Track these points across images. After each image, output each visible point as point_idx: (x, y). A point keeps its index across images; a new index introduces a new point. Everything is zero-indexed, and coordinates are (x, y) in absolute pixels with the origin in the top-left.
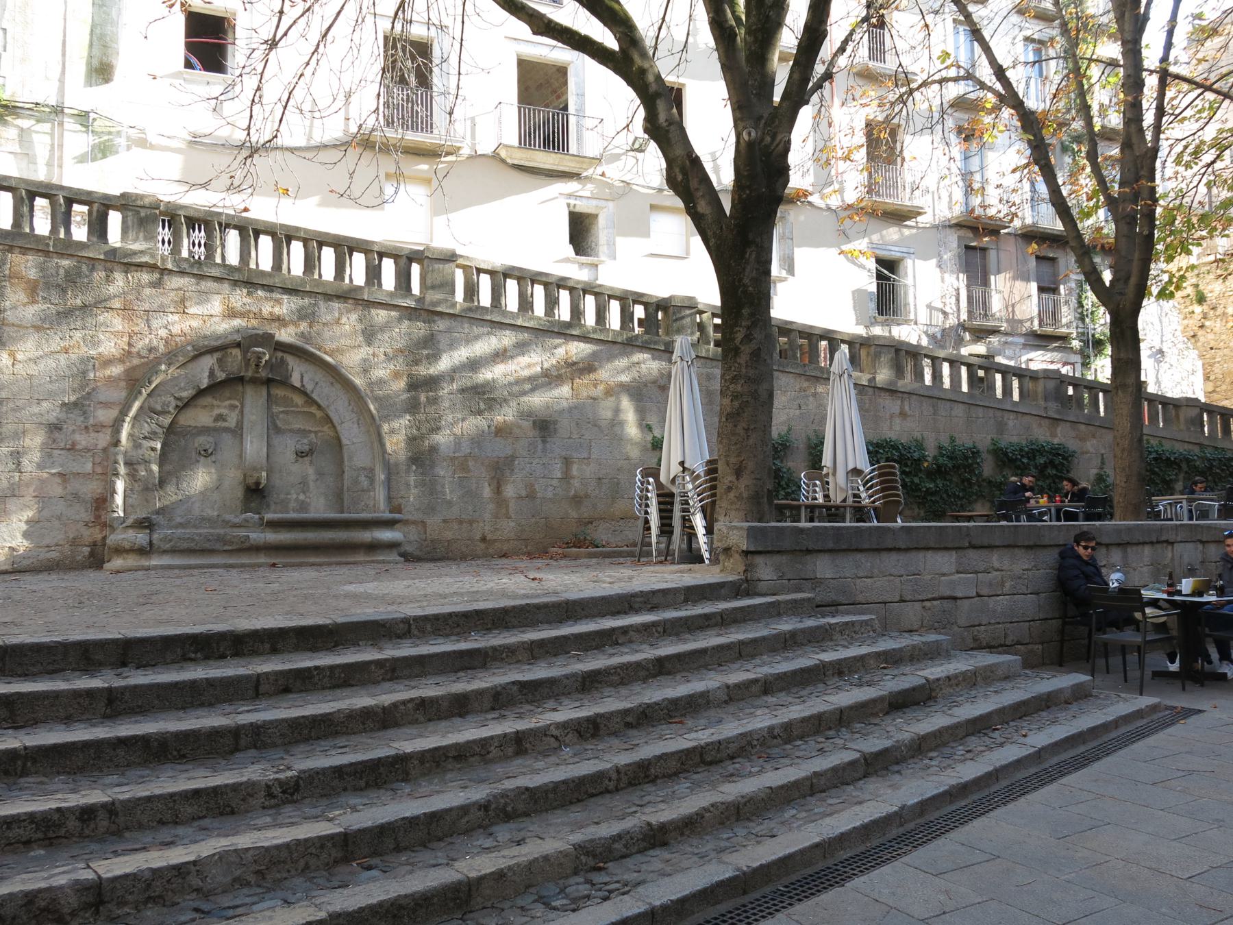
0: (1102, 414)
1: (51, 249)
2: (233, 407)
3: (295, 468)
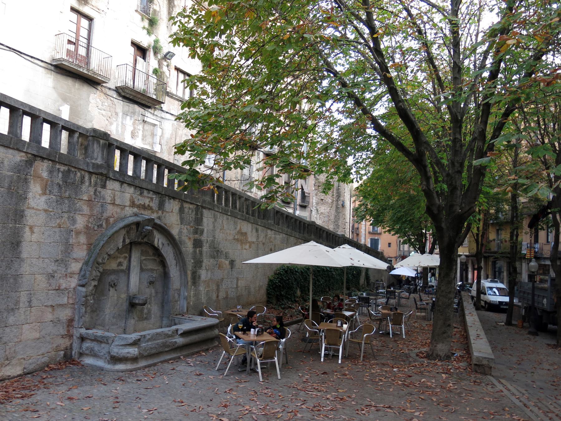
0: (165, 185)
1: (57, 160)
2: (126, 257)
3: (147, 290)
